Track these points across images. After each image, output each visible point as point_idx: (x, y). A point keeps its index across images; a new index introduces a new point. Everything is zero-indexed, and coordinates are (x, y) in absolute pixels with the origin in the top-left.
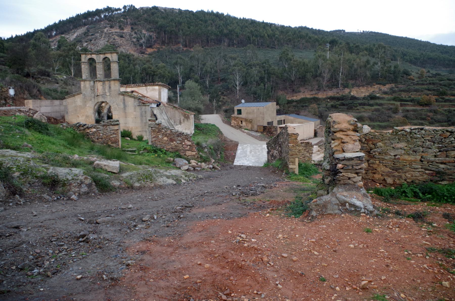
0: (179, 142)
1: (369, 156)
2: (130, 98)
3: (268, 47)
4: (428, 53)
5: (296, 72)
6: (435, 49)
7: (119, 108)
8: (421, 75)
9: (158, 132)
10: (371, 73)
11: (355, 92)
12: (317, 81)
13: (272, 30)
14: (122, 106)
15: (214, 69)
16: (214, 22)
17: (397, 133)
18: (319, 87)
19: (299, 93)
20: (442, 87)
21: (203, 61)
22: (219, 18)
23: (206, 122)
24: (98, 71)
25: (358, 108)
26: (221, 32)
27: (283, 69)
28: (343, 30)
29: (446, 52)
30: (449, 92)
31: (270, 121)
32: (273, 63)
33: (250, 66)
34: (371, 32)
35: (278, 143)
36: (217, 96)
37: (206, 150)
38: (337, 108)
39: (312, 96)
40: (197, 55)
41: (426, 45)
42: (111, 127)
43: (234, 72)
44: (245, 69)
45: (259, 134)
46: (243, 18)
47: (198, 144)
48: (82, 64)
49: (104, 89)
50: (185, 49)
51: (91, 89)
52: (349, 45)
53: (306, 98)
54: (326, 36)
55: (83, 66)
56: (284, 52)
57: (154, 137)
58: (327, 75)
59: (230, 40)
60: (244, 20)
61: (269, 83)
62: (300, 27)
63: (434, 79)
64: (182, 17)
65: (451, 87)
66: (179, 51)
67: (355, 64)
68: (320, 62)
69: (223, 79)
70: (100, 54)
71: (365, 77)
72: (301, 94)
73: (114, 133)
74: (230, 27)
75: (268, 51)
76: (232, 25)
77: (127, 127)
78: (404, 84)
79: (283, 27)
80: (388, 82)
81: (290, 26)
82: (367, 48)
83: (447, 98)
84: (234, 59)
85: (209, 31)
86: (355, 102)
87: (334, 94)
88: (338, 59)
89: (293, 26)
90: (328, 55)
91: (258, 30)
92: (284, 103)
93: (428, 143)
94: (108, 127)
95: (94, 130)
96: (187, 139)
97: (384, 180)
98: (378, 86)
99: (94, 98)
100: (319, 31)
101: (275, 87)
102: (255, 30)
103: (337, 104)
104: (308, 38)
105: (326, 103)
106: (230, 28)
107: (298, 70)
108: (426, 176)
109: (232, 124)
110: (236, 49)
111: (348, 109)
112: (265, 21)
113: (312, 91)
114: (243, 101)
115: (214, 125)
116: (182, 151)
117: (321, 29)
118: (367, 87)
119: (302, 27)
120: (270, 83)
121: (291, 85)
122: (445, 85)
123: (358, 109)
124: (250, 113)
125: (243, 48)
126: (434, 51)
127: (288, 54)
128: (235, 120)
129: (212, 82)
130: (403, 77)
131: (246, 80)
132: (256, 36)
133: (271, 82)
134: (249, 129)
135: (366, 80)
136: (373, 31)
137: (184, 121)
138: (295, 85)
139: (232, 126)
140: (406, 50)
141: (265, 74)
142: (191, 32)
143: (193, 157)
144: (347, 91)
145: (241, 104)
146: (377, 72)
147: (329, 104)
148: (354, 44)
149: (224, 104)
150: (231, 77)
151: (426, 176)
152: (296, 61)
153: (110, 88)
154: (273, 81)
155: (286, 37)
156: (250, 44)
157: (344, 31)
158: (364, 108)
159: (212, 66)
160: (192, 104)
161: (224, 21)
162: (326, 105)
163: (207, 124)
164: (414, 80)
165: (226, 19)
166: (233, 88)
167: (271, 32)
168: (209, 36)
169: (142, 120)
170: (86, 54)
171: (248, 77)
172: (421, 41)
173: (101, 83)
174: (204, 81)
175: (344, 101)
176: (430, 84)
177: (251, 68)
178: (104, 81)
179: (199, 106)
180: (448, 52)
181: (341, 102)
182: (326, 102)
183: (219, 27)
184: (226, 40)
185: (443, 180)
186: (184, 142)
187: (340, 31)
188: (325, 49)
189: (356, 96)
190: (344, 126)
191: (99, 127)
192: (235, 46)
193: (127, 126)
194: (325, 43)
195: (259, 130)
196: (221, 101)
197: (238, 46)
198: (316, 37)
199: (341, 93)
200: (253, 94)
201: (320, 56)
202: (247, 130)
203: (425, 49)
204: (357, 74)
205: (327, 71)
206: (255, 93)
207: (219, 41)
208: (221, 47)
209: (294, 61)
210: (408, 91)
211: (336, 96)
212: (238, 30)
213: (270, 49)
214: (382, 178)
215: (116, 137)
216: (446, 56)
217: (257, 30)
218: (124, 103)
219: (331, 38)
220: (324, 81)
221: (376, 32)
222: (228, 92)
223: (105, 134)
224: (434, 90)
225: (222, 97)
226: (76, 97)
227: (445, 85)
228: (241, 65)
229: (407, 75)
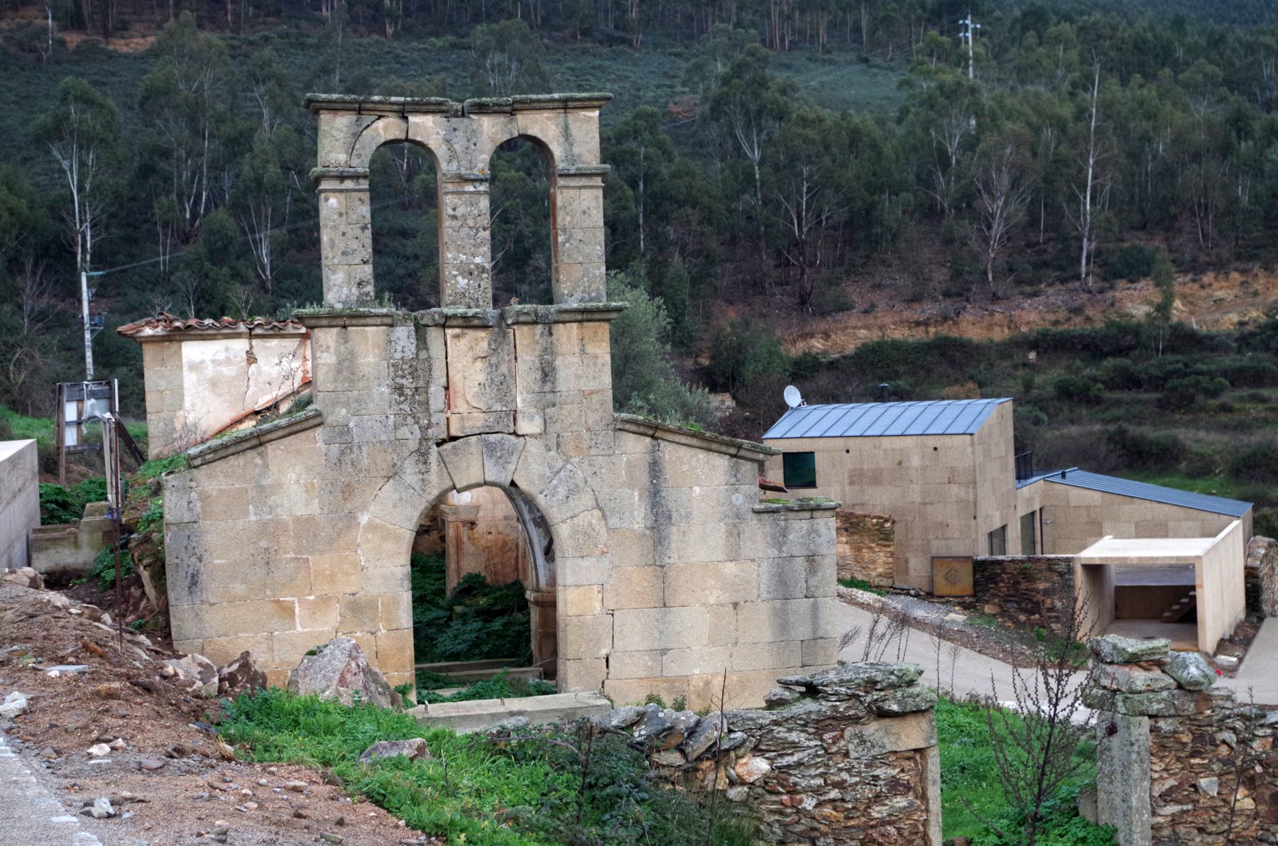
2: (702, 455)
3: (586, 33)
7: (611, 530)
9: (1195, 754)
10: (1260, 188)
14: (637, 517)
18: (957, 274)
24: (460, 249)
25: (1227, 397)
38: (1098, 401)
40: (188, 79)
42: (872, 729)
48: (324, 185)
49: (502, 386)
50: (74, 39)
51: (399, 389)
53: (895, 345)
55: (330, 205)
57: (1167, 797)
58: (1006, 203)
66: (32, 50)
70: (482, 109)
72: (853, 319)
73: (895, 786)
77: (672, 681)
82: (1145, 42)
86: (1200, 366)
87: (1053, 318)
94: (849, 732)
95: (758, 766)
99: (422, 455)
111: (1162, 405)
113: (916, 299)
114: (792, 396)
118: (1243, 272)
123: (1225, 409)
124: (876, 478)
125: (439, 43)
134: (877, 581)
153: (547, 373)
158: (1264, 400)
169: (783, 623)
170: (359, 111)
173: (481, 340)
175: (1135, 362)
178: (500, 328)
181: (1115, 369)
182: (1015, 367)
191: (794, 736)
192: (390, 30)
193: (674, 670)
195: (942, 587)
197: (408, 30)
205: (1003, 181)
213: (604, 50)
215: (908, 811)
218: (655, 496)
223: (834, 794)
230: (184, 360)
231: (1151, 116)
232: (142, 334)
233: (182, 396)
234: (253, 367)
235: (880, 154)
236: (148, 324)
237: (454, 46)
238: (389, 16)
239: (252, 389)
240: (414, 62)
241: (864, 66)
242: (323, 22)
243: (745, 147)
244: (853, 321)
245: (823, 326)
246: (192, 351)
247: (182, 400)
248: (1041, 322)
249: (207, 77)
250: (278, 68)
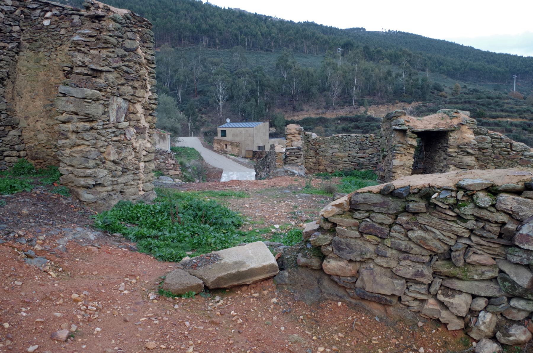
0: (162, 161)
1: (316, 154)
3: (262, 49)
4: (471, 62)
5: (298, 84)
6: (480, 57)
8: (455, 91)
11: (373, 111)
12: (325, 96)
13: (268, 27)
15: (189, 78)
16: (188, 13)
17: (333, 138)
18: (327, 104)
19: (302, 112)
20: (479, 106)
21: (174, 66)
22: (196, 7)
23: (184, 146)
26: (199, 27)
27: (281, 80)
29: (494, 62)
30: (488, 113)
31: (261, 145)
32: (268, 71)
33: (238, 75)
34: (399, 32)
35: (266, 164)
36: (194, 113)
37: (190, 170)
39: (318, 116)
40: (166, 58)
41: (469, 52)
43: (216, 83)
44: (231, 79)
45: (247, 161)
46: (229, 8)
47: (181, 164)
52: (369, 49)
53: (311, 118)
54: (340, 35)
56: (282, 58)
59: (211, 38)
60: (230, 12)
61: (262, 98)
62: (305, 23)
63: (471, 96)
64: (144, 4)
65: (489, 107)
67: (374, 75)
68: (329, 71)
69: (200, 91)
71: (386, 92)
72: (304, 113)
74: (211, 20)
76: (213, 17)
78: (434, 102)
79: (282, 22)
81: (292, 20)
83: (484, 120)
84: (217, 65)
85: (182, 25)
86: (372, 125)
88: (352, 69)
89: (296, 21)
90: (340, 62)
91: (249, 26)
92: (281, 124)
93: (353, 145)
96: (171, 157)
97: (326, 170)
98: (402, 103)
100: (331, 28)
101: (270, 103)
102: (245, 26)
103: (350, 127)
104: (314, 38)
105: (336, 125)
106: (211, 22)
107: (301, 81)
108: (351, 166)
109: (214, 149)
112: (258, 13)
113: (318, 109)
114: (228, 120)
115: (193, 149)
116: (165, 170)
117: (334, 26)
118: (388, 105)
119: (308, 22)
120: (263, 97)
121: (291, 101)
122: (483, 105)
125: (227, 50)
126: (479, 60)
127: (287, 61)
128: (218, 143)
129: (185, 95)
130: (433, 93)
131: (232, 93)
132: (246, 34)
133: (265, 96)
135: (386, 96)
136: (402, 30)
137: (159, 142)
138: (296, 101)
139: (215, 151)
140: (443, 57)
141: (257, 86)
142: (157, 26)
143: (177, 176)
144: (362, 110)
145: (226, 124)
146: (401, 86)
147: (340, 127)
148: (376, 48)
149: (203, 124)
150: (212, 88)
151: (351, 166)
152: (297, 70)
154: (267, 96)
155: (286, 37)
156: (238, 44)
157: (364, 29)
159: (186, 74)
160: (169, 122)
161: (202, 12)
162: (336, 128)
163: (184, 147)
164: (446, 97)
165: (206, 10)
166: (215, 104)
167: (266, 29)
168: (182, 33)
171: (234, 89)
172: (462, 46)
174: (175, 93)
176: (465, 102)
177: (239, 78)
179: (175, 126)
180: (496, 62)
183: (196, 19)
184: (206, 39)
185: (362, 168)
186: (168, 160)
188: (336, 54)
189: (374, 116)
190: (293, 131)
192: (217, 47)
194: (337, 45)
195: (247, 156)
196: (199, 121)
197: (222, 47)
198: (326, 37)
199: (355, 113)
200: (241, 112)
201: (328, 64)
202: (233, 155)
203: (467, 56)
204: (375, 89)
205: (337, 83)
206: (244, 111)
207: (195, 40)
208: (198, 49)
209: (295, 69)
211: (348, 116)
212: (221, 25)
213: (265, 53)
214: (324, 168)
216: (493, 66)
217: (247, 26)
219: (345, 40)
220: (333, 97)
221: (406, 32)
222: (208, 108)
225: (200, 115)
227: (483, 105)
228: (225, 73)
229: (438, 90)
244: (304, 113)
245: (297, 114)
249: (170, 58)
250: (185, 56)
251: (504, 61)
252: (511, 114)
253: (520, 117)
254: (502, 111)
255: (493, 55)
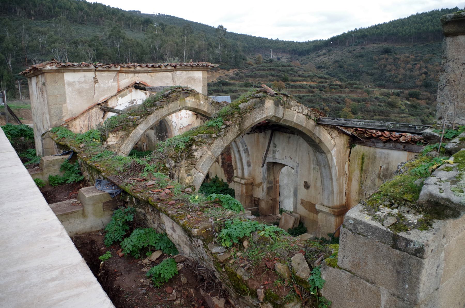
6: (228, 36)
28: (138, 11)
34: (167, 15)
75: (79, 27)
80: (231, 67)
98: (223, 70)
110: (35, 22)
118: (211, 72)
125: (45, 22)
157: (140, 12)
176: (270, 69)
187: (136, 12)
192: (33, 18)
210: (254, 77)
213: (80, 25)
221: (172, 15)
224: (277, 76)
226: (372, 148)
230: (65, 81)
231: (193, 43)
232: (45, 69)
233: (65, 97)
234: (97, 84)
235: (142, 47)
236: (48, 64)
237: (48, 22)
238: (33, 15)
239: (96, 94)
240: (39, 25)
241: (131, 32)
242: (17, 16)
243: (116, 44)
246: (69, 77)
247: (65, 99)
248: (431, 69)
251: (244, 39)
252: (306, 79)
253: (312, 81)
254: (299, 76)
255: (236, 35)
